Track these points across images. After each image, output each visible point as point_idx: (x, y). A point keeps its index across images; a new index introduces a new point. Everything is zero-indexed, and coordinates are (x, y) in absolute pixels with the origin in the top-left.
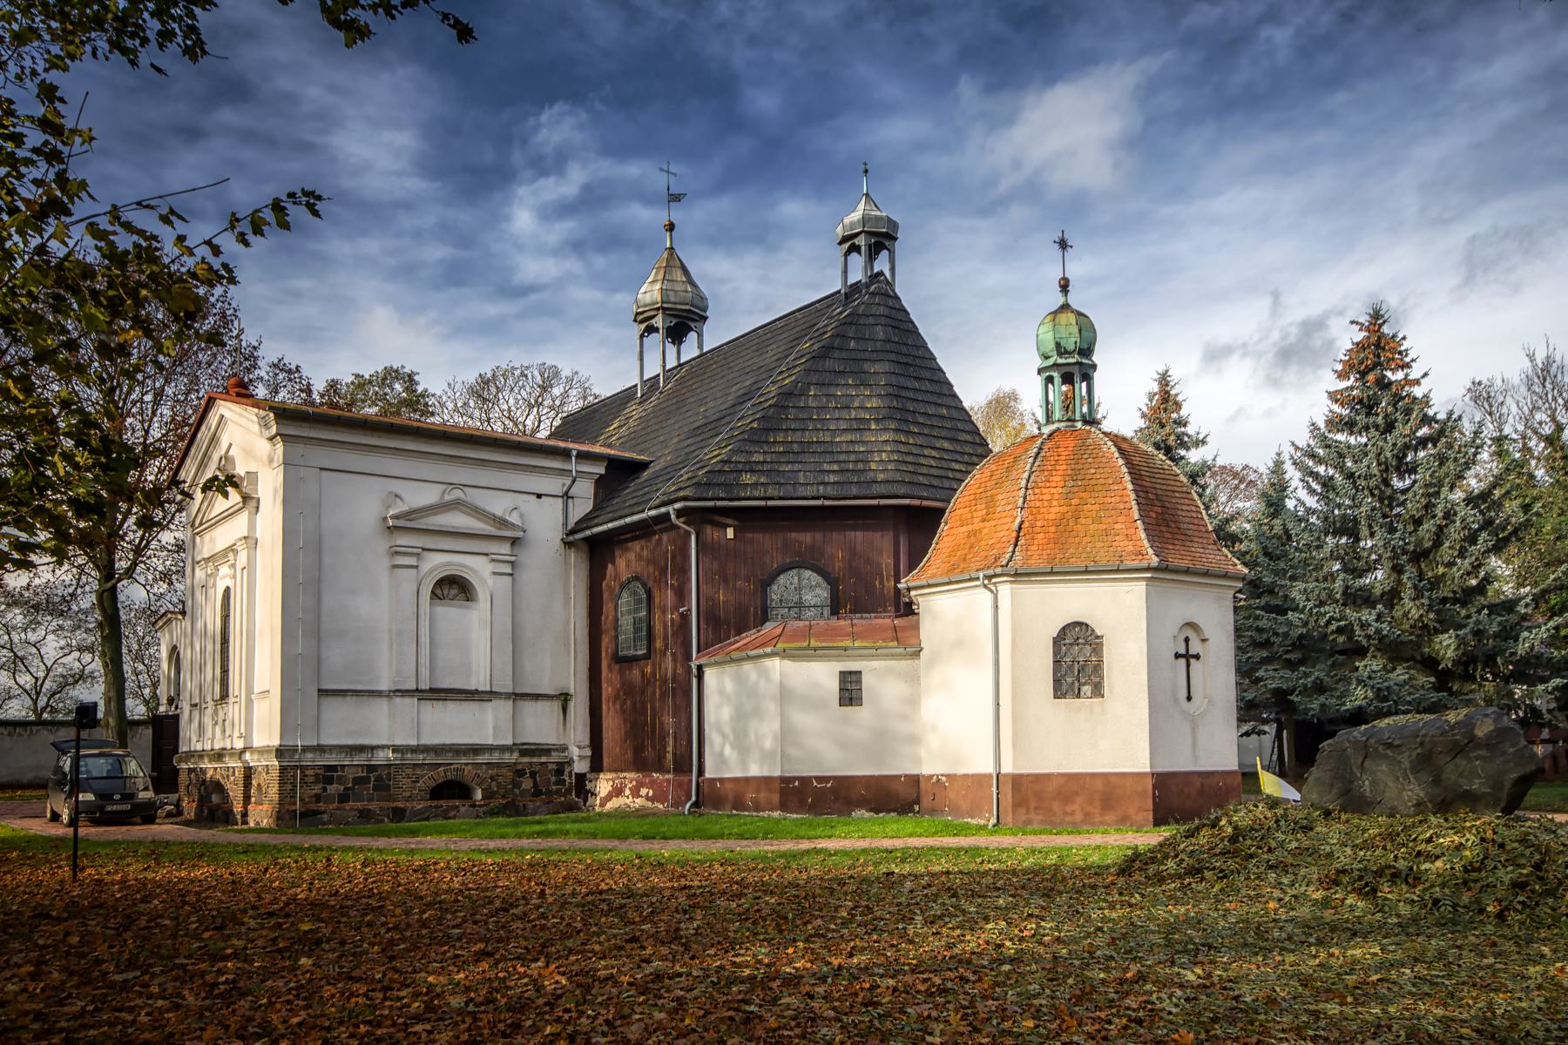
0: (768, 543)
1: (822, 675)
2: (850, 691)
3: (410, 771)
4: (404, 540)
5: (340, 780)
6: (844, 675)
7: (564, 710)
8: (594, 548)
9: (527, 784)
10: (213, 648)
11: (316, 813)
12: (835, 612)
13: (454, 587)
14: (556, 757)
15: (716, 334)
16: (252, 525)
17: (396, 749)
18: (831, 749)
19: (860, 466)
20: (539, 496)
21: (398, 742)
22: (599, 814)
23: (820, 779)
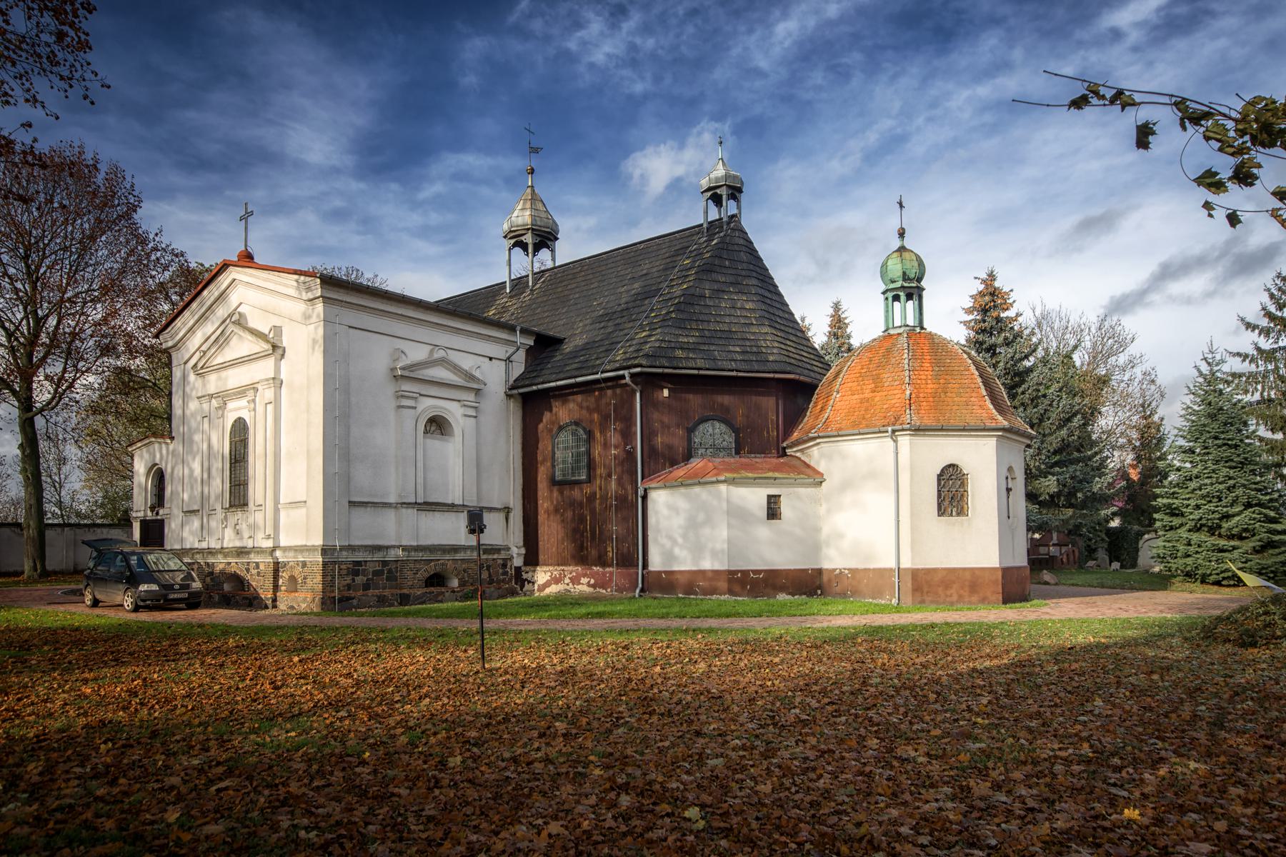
0: (695, 400)
1: (754, 497)
2: (773, 511)
3: (412, 565)
4: (407, 386)
5: (364, 573)
6: (769, 497)
7: (507, 519)
8: (531, 401)
9: (485, 575)
10: (220, 467)
11: (349, 599)
12: (737, 452)
13: (438, 425)
14: (503, 555)
15: (567, 251)
16: (277, 369)
17: (405, 548)
18: (771, 550)
19: (755, 349)
20: (491, 359)
21: (404, 543)
22: (539, 599)
23: (755, 572)
